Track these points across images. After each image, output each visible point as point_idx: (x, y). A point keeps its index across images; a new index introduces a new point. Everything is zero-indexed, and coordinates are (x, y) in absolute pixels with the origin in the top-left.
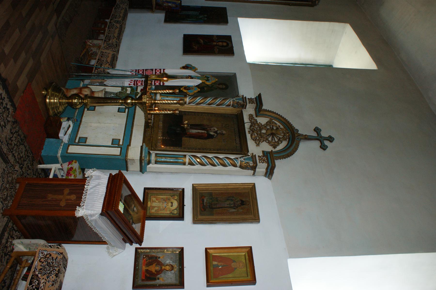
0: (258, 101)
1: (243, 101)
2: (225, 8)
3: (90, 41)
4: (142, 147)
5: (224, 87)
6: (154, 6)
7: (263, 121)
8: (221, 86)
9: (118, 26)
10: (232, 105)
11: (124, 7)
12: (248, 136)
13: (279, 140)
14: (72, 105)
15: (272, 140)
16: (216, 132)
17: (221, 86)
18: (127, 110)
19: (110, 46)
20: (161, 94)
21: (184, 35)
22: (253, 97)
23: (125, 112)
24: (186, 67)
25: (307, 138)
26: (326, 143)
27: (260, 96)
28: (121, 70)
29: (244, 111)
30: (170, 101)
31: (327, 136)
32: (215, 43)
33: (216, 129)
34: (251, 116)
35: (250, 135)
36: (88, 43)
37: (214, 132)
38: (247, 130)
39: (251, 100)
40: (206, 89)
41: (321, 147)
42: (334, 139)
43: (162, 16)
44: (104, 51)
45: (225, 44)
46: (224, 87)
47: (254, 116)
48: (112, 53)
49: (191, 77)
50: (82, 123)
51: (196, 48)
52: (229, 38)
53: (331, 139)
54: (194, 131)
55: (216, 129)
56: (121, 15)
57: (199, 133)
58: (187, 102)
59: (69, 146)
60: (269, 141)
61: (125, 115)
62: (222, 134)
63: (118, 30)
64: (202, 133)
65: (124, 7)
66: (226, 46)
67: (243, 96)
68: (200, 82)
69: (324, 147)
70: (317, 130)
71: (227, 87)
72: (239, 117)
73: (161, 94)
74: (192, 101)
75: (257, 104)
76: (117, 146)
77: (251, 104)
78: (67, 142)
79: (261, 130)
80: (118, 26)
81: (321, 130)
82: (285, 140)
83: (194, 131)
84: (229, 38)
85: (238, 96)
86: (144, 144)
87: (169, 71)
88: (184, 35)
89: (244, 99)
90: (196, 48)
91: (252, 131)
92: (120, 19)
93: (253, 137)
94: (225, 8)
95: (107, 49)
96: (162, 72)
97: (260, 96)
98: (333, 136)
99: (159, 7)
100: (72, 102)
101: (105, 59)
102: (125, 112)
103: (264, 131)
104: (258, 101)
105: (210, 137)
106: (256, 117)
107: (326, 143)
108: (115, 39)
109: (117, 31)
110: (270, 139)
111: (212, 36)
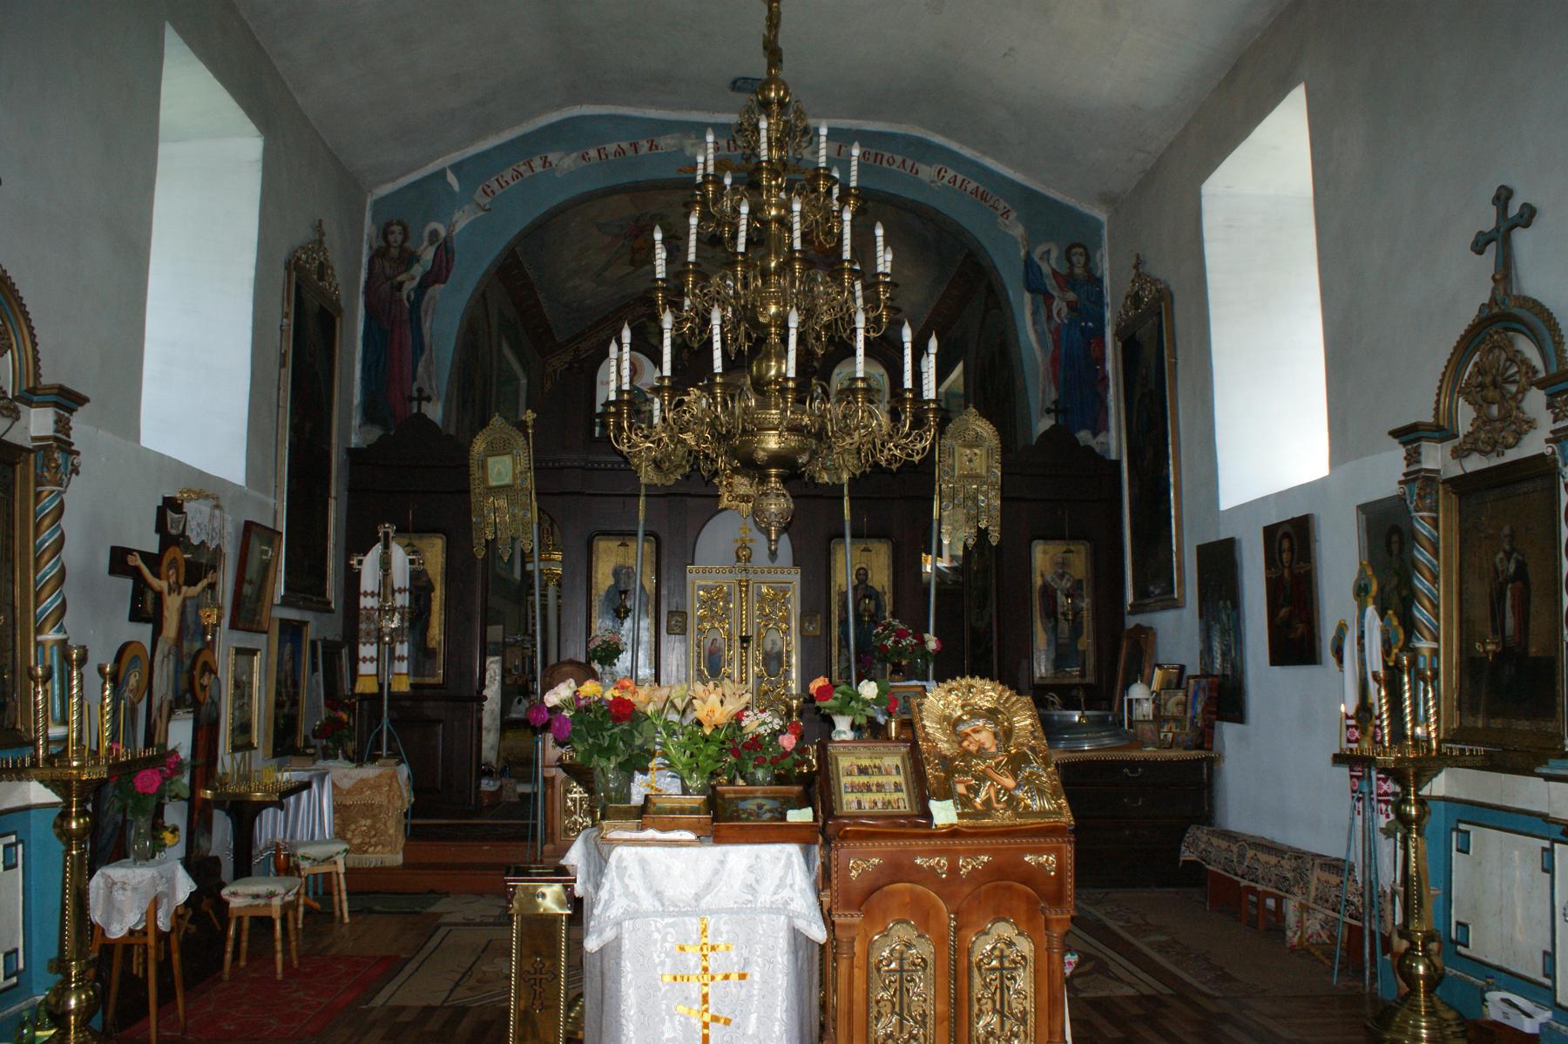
0: (1409, 436)
1: (1414, 480)
2: (1200, 548)
3: (1289, 933)
4: (1548, 778)
5: (1395, 538)
6: (1202, 754)
7: (1465, 418)
8: (1395, 547)
9: (1250, 853)
10: (1430, 510)
11: (1205, 838)
12: (1511, 455)
13: (1512, 360)
14: (1435, 979)
15: (1514, 382)
16: (1508, 555)
17: (1395, 547)
18: (1462, 826)
19: (1301, 878)
20: (1415, 723)
21: (1273, 662)
22: (1401, 452)
23: (1468, 833)
24: (1339, 653)
25: (1505, 271)
26: (1514, 209)
27: (1395, 434)
28: (1349, 839)
29: (1445, 475)
30: (1426, 702)
31: (1493, 211)
32: (1286, 572)
33: (1501, 555)
34: (1458, 454)
35: (1508, 452)
36: (1296, 940)
37: (1509, 560)
38: (1495, 461)
39: (1413, 457)
40: (1404, 593)
41: (1527, 225)
42: (1502, 187)
43: (1228, 732)
44: (1313, 893)
45: (1286, 544)
46: (1395, 538)
47: (1456, 442)
48: (1317, 872)
49: (1361, 637)
50: (1505, 966)
51: (1301, 628)
52: (1270, 532)
53: (1503, 197)
54: (1510, 622)
55: (1501, 555)
56: (1224, 844)
57: (1513, 607)
58: (1434, 645)
59: (1559, 1006)
60: (1518, 392)
61: (1475, 832)
62: (1512, 536)
63: (1261, 856)
64: (1513, 595)
65: (1205, 838)
66: (1291, 539)
67: (1400, 483)
68: (1371, 610)
69: (1528, 216)
70: (1479, 247)
71: (1395, 529)
72: (1463, 486)
73: (1415, 723)
74: (1426, 633)
75: (1419, 439)
76: (351, 430)
77: (1423, 458)
78: (1549, 1014)
79: (1490, 421)
80: (1250, 853)
81: (1481, 233)
82: (1511, 342)
83: (1510, 622)
84: (1270, 532)
85: (1401, 498)
86: (1538, 770)
87: (1348, 706)
88: (1273, 662)
89: (1409, 479)
90: (1301, 628)
91: (1495, 446)
92: (1235, 848)
93: (1511, 440)
94: (1200, 548)
95: (1306, 885)
96: (1352, 722)
97: (1395, 434)
98: (1493, 194)
99: (1205, 738)
100: (1426, 978)
101: (1334, 892)
102: (1468, 833)
103: (1495, 410)
104: (1412, 436)
105: (1521, 574)
106: (1456, 436)
107: (1514, 209)
108: (1283, 862)
109: (1263, 857)
110: (1513, 388)
111: (1268, 580)
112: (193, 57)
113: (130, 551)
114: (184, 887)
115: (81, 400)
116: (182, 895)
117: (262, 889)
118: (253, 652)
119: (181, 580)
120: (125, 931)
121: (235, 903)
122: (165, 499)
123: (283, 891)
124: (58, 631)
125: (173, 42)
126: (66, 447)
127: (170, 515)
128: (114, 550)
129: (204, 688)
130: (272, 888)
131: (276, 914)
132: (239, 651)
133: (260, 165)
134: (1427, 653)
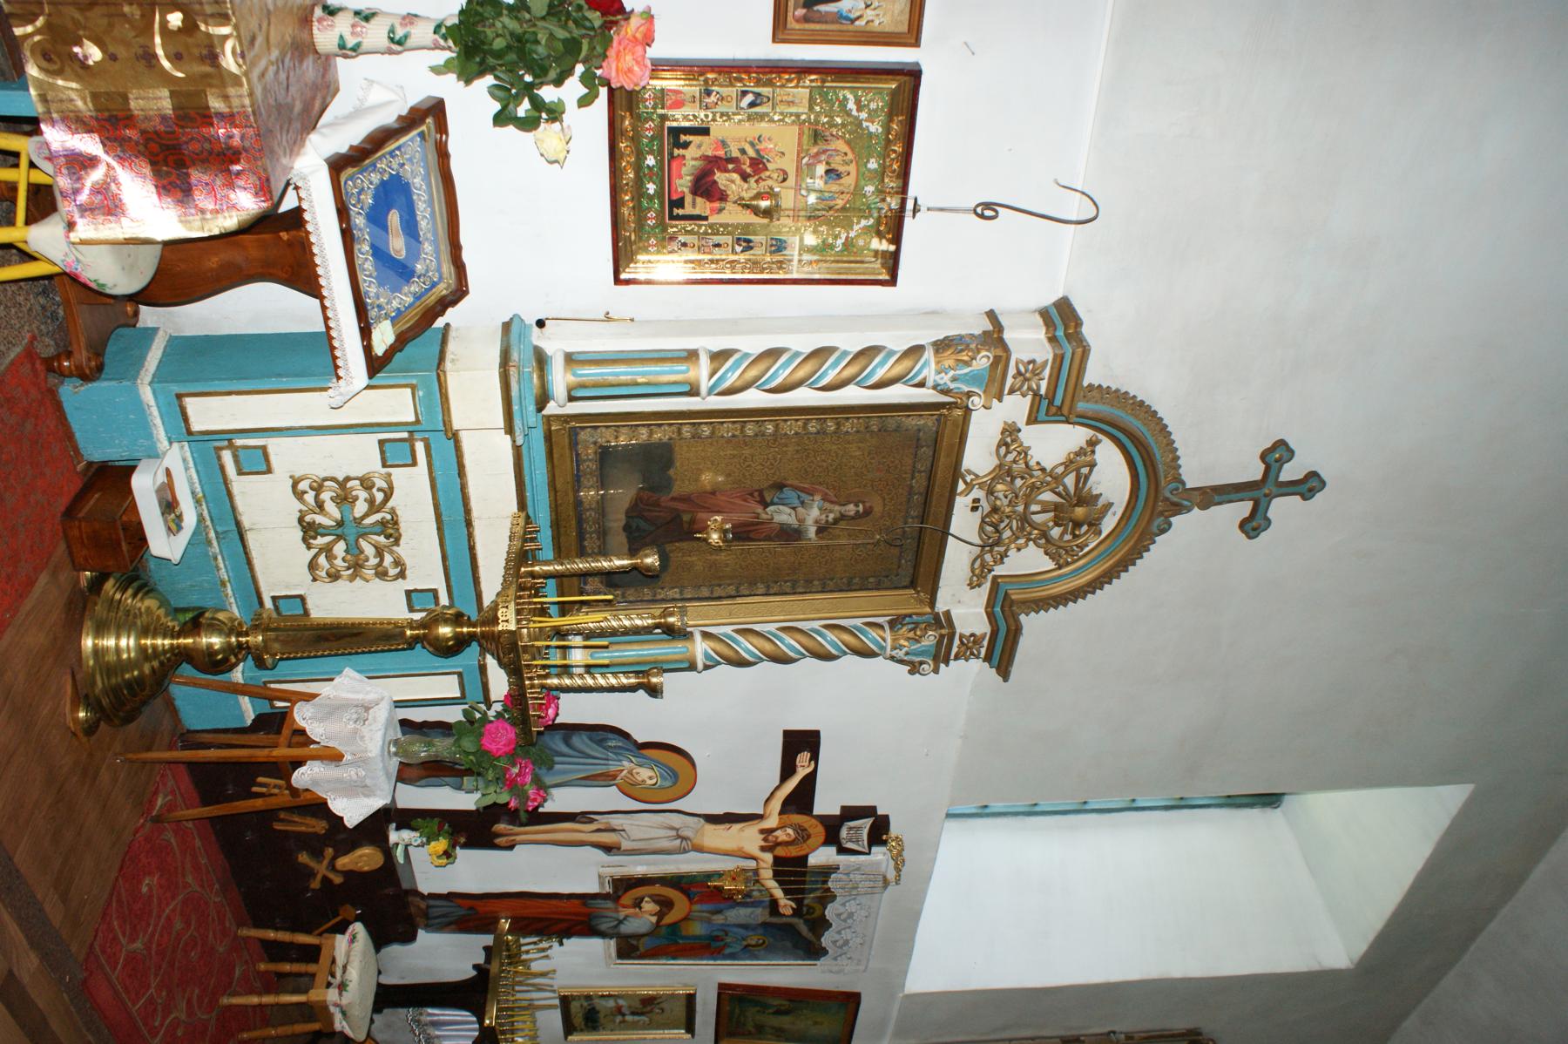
88: (787, 734)
112: (1435, 835)
113: (815, 757)
114: (352, 810)
115: (1004, 670)
116: (338, 806)
117: (353, 974)
118: (690, 1028)
119: (780, 852)
120: (302, 723)
121: (341, 941)
122: (886, 817)
123: (344, 1001)
124: (707, 656)
125: (1449, 799)
126: (941, 656)
127: (866, 823)
128: (815, 735)
129: (638, 904)
130: (353, 986)
131: (314, 995)
132: (690, 999)
133: (1315, 967)
134: (691, 375)
